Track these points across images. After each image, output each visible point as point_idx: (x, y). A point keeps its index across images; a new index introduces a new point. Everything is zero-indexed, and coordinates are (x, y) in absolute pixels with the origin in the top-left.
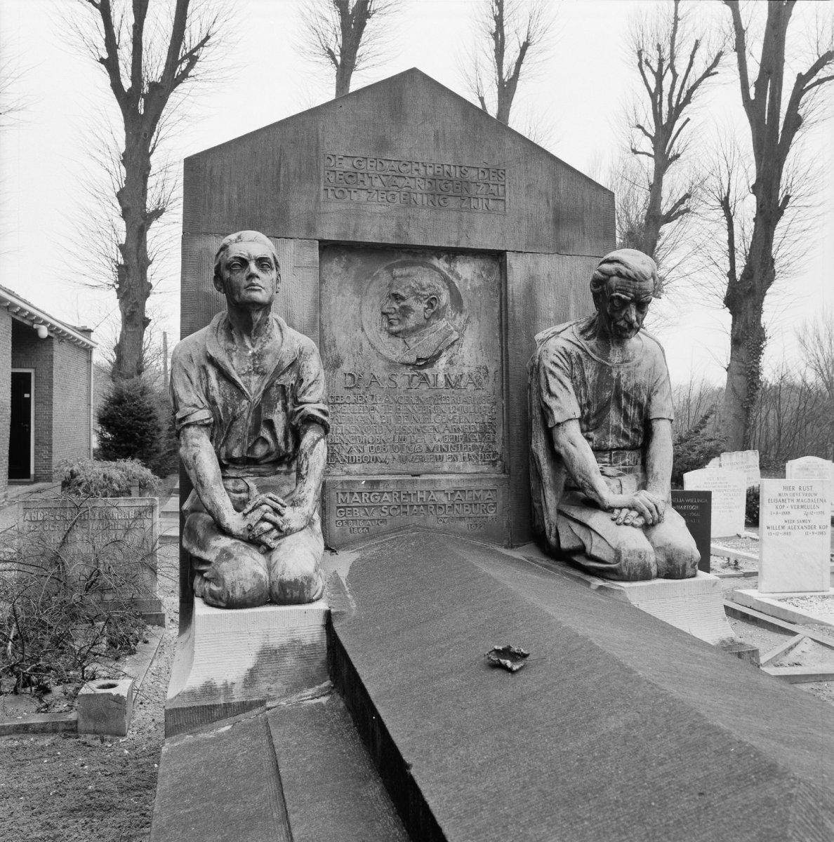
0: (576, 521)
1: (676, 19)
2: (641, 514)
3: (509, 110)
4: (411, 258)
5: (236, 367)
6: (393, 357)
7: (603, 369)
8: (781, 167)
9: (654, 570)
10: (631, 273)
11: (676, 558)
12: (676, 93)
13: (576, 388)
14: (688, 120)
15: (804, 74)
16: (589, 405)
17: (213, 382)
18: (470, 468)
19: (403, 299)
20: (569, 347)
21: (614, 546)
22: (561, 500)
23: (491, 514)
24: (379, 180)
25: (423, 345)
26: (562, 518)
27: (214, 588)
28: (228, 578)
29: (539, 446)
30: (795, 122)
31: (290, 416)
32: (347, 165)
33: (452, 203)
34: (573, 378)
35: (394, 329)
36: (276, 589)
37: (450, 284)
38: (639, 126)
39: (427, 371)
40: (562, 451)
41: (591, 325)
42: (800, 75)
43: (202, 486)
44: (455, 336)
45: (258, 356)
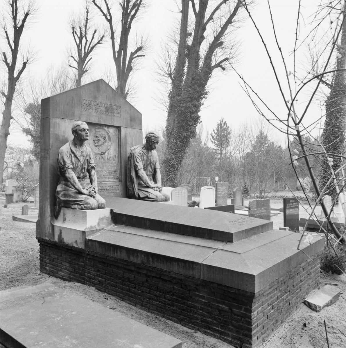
1: (87, 19)
2: (159, 188)
3: (19, 40)
4: (99, 127)
5: (78, 154)
6: (96, 152)
7: (148, 157)
8: (126, 83)
12: (87, 47)
13: (142, 161)
14: (91, 58)
15: (133, 52)
16: (145, 165)
17: (73, 158)
18: (112, 180)
19: (98, 137)
20: (141, 152)
22: (138, 186)
23: (118, 191)
25: (102, 149)
26: (139, 191)
29: (133, 174)
30: (130, 69)
31: (88, 166)
32: (87, 102)
33: (110, 114)
34: (141, 159)
35: (96, 145)
36: (100, 205)
37: (108, 134)
38: (72, 57)
39: (103, 156)
40: (140, 175)
41: (144, 147)
42: (132, 52)
43: (75, 183)
44: (109, 147)
45: (82, 152)
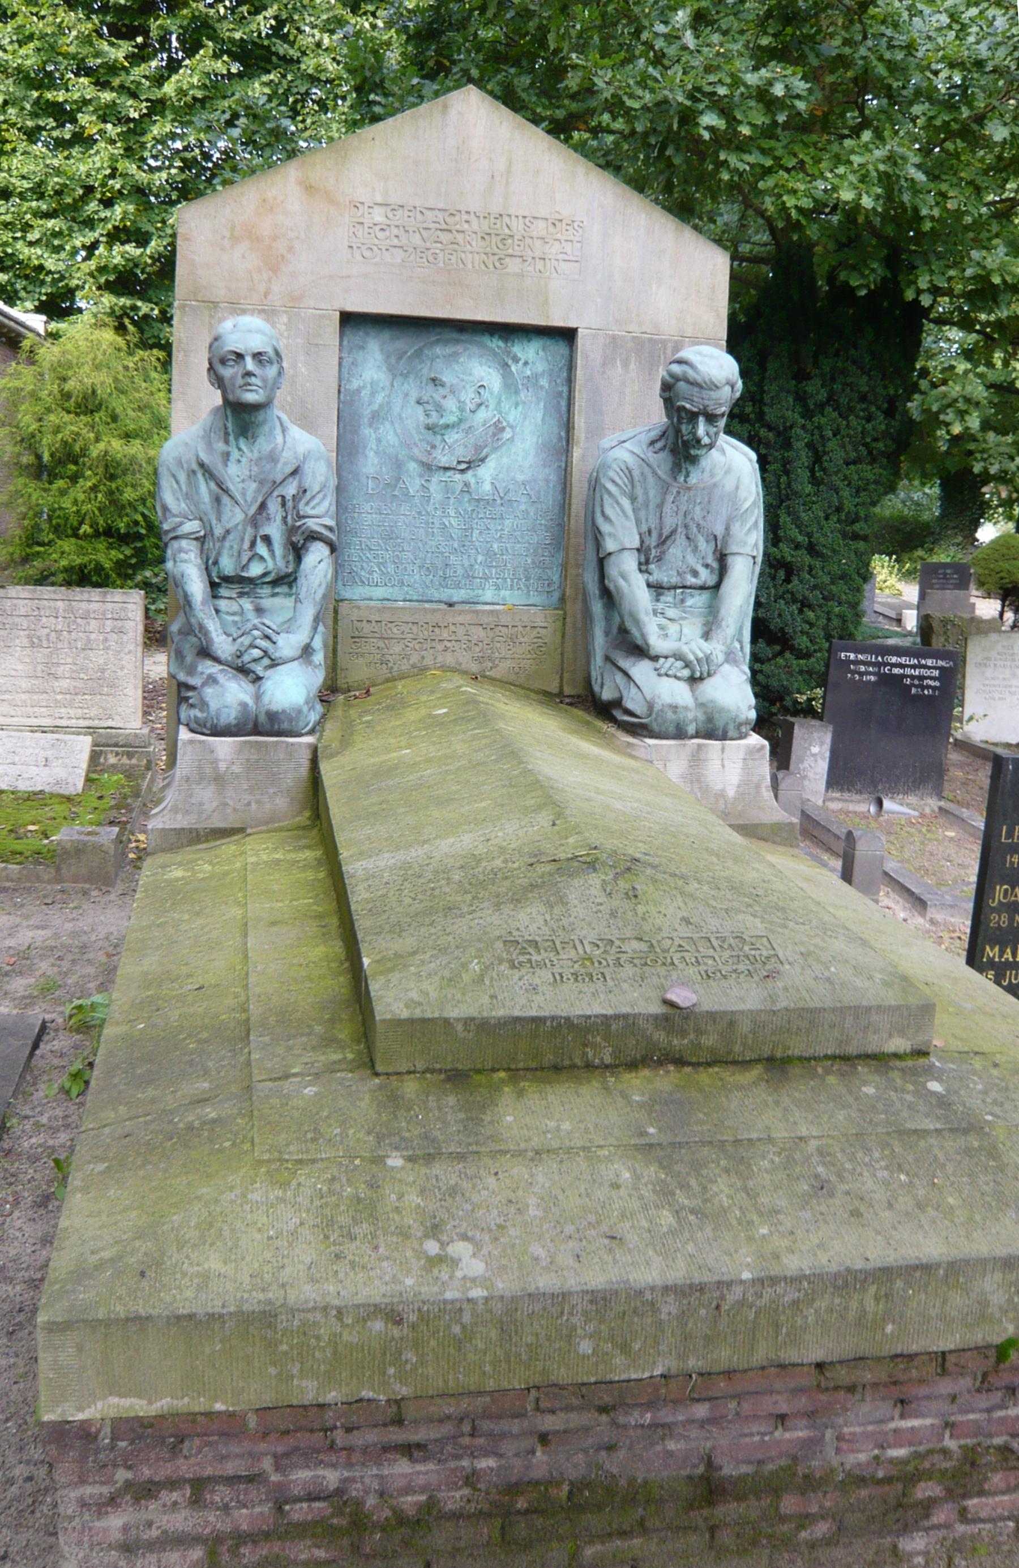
0: (620, 669)
2: (687, 665)
9: (691, 729)
10: (699, 380)
11: (716, 716)
21: (648, 698)
24: (417, 235)
26: (609, 665)
27: (199, 715)
28: (214, 705)
34: (633, 499)
